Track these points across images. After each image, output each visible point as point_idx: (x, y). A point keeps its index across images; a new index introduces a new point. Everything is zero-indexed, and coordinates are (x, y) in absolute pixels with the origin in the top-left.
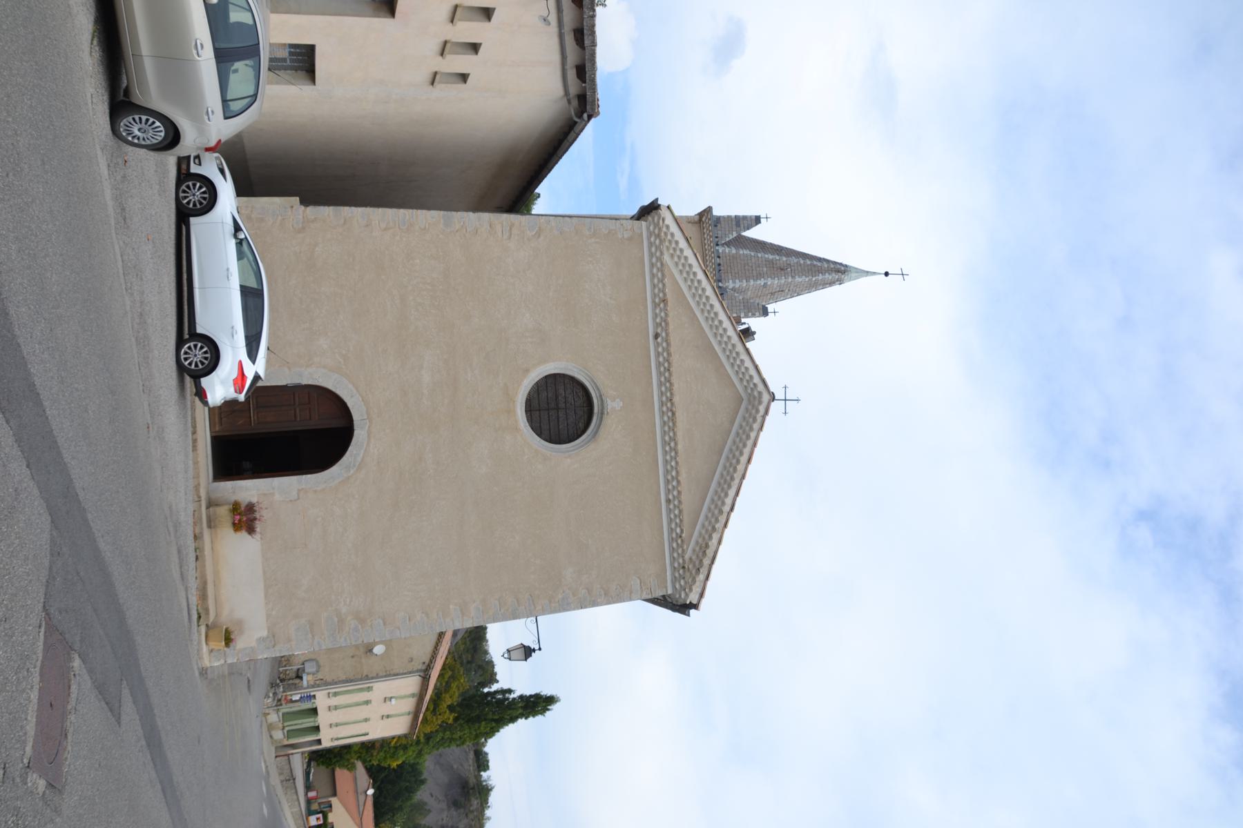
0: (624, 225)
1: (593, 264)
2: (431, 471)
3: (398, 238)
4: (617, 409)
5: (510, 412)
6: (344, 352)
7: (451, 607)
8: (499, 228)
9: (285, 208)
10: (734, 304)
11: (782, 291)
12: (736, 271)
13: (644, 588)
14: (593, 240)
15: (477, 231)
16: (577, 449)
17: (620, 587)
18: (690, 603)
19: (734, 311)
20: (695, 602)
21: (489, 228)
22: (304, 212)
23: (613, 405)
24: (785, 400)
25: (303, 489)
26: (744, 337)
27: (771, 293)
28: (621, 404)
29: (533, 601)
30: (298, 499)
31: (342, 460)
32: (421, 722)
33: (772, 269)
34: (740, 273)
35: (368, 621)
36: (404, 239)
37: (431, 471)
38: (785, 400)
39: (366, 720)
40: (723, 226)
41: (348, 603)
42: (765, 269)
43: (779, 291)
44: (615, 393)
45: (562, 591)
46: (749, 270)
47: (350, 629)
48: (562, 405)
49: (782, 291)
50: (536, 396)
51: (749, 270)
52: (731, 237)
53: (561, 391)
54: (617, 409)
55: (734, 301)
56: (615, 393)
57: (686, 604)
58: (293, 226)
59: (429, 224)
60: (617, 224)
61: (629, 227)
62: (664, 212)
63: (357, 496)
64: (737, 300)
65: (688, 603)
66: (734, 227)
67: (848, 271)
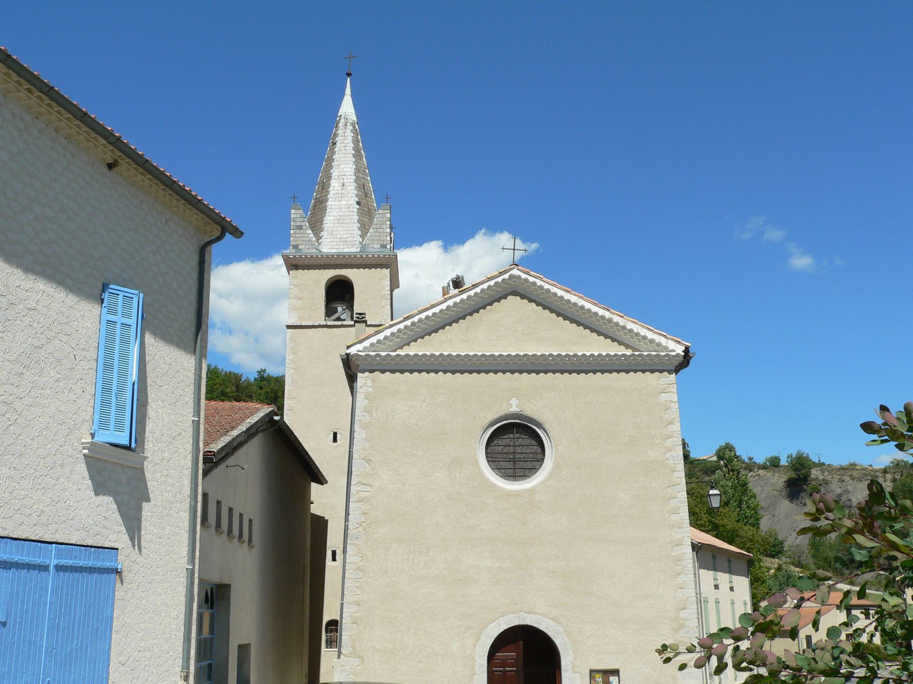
0: (361, 385)
1: (395, 415)
2: (563, 563)
3: (370, 580)
4: (518, 403)
5: (517, 494)
6: (463, 629)
7: (673, 554)
8: (362, 494)
9: (343, 671)
10: (378, 238)
11: (364, 186)
12: (345, 232)
13: (668, 390)
14: (374, 414)
15: (365, 513)
16: (549, 438)
17: (666, 410)
18: (683, 352)
19: (384, 238)
20: (683, 348)
21: (362, 503)
22: (346, 656)
23: (514, 407)
24: (514, 249)
25: (573, 669)
26: (461, 287)
27: (366, 197)
28: (514, 399)
29: (673, 486)
30: (580, 672)
31: (550, 636)
32: (730, 543)
33: (343, 195)
34: (346, 229)
35: (681, 622)
36: (371, 575)
37: (563, 563)
38: (514, 249)
39: (733, 603)
40: (301, 243)
41: (665, 638)
42: (343, 203)
43: (364, 189)
44: (505, 404)
45: (667, 461)
46: (344, 219)
47: (686, 637)
48: (511, 449)
49: (364, 186)
50: (502, 471)
51: (344, 219)
52: (312, 235)
53: (500, 449)
54: (518, 403)
55: (375, 238)
56: (505, 404)
57: (684, 356)
58: (358, 666)
59: (358, 553)
60: (361, 391)
61: (364, 381)
62: (353, 351)
63: (581, 626)
64: (374, 234)
65: (683, 354)
66: (302, 231)
67: (345, 115)
